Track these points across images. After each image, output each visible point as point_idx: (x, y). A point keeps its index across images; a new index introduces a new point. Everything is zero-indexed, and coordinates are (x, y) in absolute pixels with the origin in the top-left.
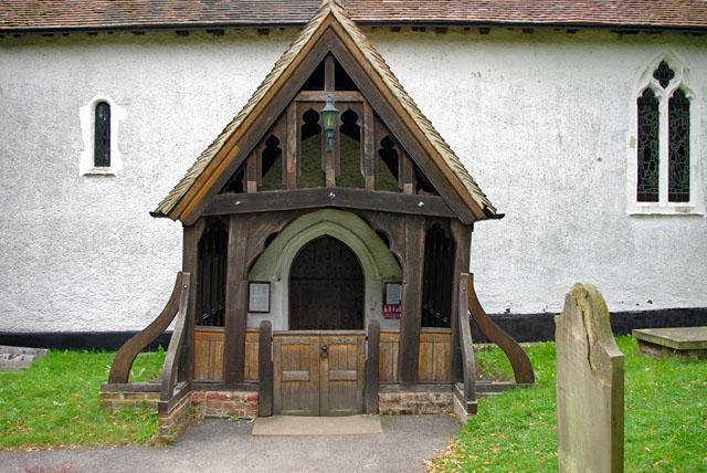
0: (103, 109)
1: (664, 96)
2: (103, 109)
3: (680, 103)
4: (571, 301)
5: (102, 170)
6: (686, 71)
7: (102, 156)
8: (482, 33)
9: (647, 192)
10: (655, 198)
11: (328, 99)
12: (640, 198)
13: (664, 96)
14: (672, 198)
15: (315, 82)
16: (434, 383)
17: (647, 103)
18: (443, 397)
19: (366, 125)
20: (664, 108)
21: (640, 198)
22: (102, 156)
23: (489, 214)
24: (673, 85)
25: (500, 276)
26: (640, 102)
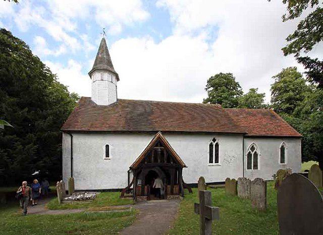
0: (107, 146)
1: (214, 144)
2: (107, 146)
3: (217, 145)
4: (226, 180)
5: (108, 158)
6: (218, 140)
7: (107, 155)
8: (193, 37)
9: (211, 161)
10: (212, 162)
11: (159, 148)
12: (210, 162)
13: (214, 144)
14: (215, 162)
15: (157, 146)
16: (176, 194)
17: (211, 145)
18: (178, 196)
19: (165, 153)
20: (214, 146)
21: (210, 162)
22: (107, 155)
23: (185, 166)
24: (216, 142)
25: (188, 177)
26: (210, 145)
